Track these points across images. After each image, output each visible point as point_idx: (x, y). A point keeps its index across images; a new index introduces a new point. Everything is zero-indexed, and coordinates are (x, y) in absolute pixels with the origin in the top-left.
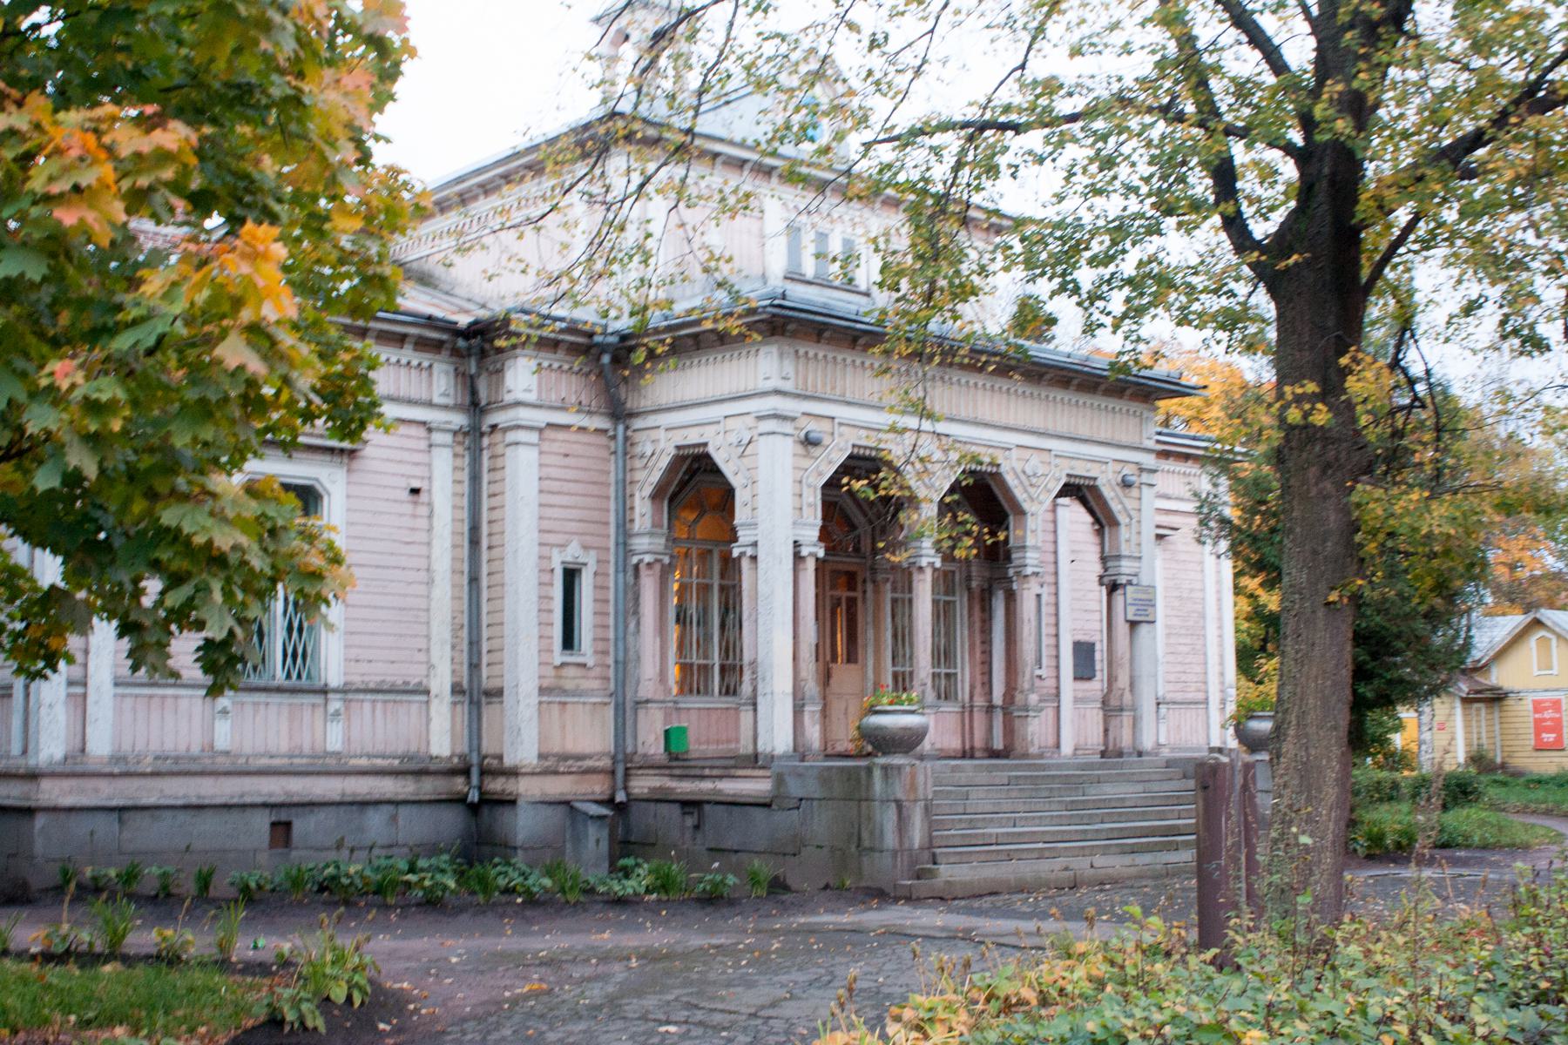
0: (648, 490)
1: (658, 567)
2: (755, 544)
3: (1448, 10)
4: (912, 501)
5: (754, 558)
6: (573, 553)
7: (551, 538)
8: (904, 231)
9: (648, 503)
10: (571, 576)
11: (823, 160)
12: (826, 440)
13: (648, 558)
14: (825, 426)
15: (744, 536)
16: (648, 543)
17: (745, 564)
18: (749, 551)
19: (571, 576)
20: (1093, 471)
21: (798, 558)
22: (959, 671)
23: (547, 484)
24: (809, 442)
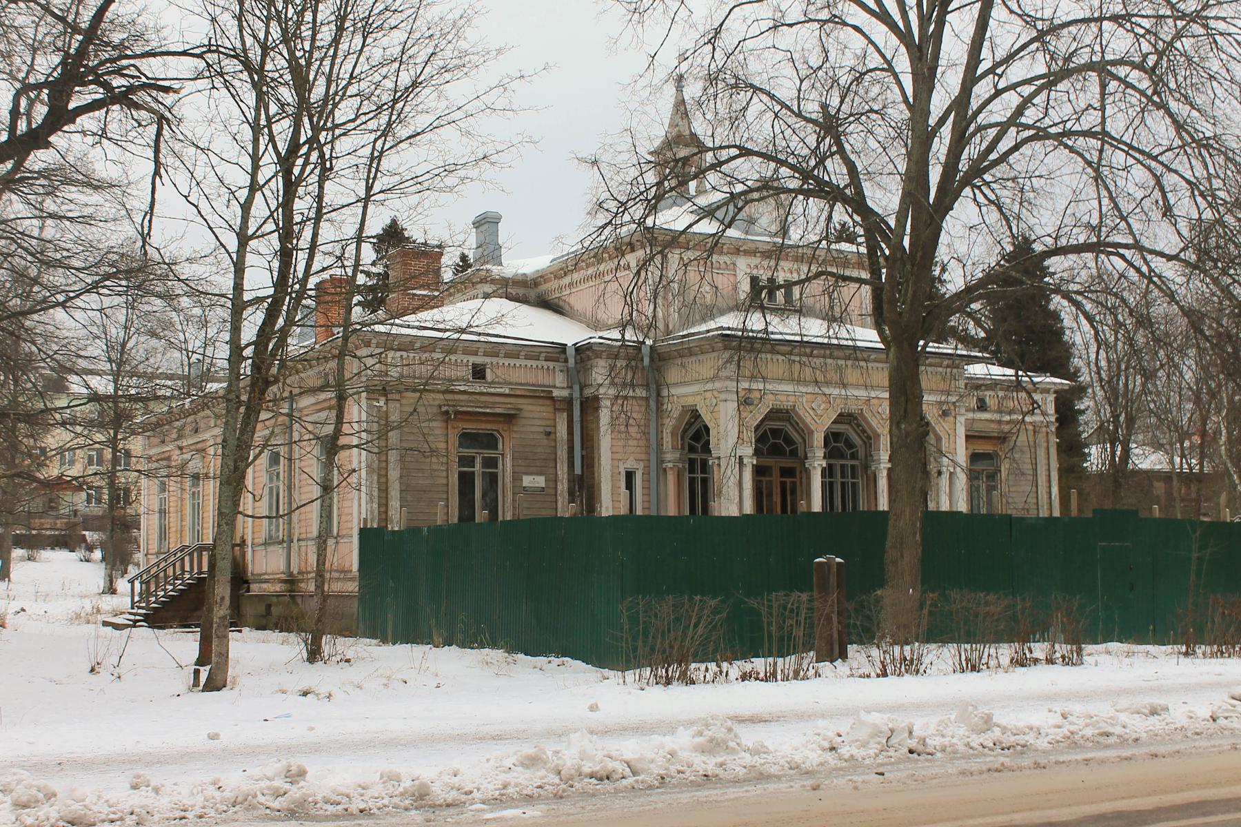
1: (676, 469)
2: (719, 458)
6: (630, 464)
9: (670, 435)
10: (630, 476)
13: (670, 465)
16: (671, 456)
19: (630, 476)
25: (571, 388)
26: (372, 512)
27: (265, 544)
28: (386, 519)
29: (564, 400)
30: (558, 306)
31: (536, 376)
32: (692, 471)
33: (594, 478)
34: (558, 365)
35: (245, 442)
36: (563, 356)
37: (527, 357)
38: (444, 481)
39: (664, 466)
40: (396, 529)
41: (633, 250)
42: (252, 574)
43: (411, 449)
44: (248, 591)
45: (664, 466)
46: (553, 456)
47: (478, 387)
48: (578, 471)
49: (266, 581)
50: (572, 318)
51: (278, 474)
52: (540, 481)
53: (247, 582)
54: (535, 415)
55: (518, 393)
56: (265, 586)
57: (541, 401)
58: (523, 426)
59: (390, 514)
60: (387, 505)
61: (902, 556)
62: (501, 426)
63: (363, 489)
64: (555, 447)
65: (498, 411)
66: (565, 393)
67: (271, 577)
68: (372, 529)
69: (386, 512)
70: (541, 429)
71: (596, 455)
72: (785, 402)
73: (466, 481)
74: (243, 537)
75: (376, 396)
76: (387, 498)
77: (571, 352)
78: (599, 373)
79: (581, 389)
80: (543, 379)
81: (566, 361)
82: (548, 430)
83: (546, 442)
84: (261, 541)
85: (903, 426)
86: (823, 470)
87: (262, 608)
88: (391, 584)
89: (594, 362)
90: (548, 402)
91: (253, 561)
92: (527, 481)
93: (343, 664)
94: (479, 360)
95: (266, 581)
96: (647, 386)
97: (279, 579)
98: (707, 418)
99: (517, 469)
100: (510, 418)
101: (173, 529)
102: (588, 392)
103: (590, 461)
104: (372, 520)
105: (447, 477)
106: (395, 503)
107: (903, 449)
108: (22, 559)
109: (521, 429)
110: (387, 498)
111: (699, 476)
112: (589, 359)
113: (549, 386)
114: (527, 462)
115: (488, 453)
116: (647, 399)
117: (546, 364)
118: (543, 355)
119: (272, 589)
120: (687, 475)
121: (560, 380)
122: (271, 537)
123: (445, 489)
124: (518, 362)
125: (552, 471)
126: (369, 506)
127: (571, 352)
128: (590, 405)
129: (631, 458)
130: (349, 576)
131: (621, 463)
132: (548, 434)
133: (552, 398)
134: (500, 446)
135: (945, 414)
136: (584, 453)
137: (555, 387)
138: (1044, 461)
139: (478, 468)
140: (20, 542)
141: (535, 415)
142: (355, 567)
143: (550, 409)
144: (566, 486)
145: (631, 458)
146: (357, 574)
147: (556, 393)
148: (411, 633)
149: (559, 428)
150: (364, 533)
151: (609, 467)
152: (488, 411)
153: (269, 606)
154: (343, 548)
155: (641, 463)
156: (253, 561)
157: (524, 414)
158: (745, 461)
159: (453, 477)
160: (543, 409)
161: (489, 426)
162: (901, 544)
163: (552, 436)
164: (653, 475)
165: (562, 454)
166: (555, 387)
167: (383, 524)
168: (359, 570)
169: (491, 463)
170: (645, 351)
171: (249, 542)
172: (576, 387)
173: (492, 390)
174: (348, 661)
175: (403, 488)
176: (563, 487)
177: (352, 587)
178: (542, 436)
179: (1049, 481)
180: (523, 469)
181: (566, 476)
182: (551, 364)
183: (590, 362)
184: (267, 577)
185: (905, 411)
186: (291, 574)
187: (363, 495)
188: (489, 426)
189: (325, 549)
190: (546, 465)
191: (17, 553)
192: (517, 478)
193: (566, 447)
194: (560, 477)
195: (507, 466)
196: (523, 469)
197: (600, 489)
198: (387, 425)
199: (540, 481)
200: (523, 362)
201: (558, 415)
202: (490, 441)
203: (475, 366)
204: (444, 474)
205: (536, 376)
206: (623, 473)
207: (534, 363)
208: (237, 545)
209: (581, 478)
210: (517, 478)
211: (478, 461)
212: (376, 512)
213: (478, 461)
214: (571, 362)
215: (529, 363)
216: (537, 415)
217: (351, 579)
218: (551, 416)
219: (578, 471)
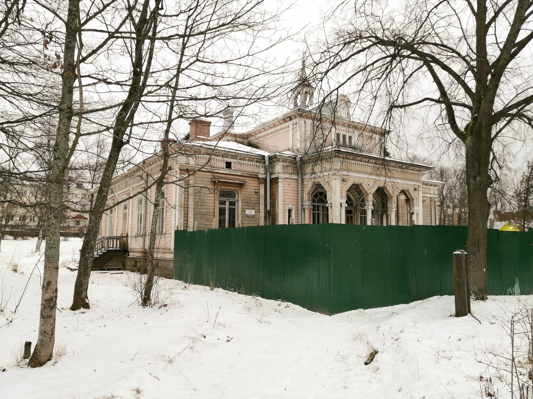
0: (306, 192)
1: (309, 209)
2: (331, 204)
3: (68, 1)
4: (367, 194)
5: (331, 207)
6: (290, 206)
7: (285, 203)
8: (6, 66)
9: (307, 195)
10: (290, 211)
11: (157, 78)
12: (348, 180)
13: (307, 207)
14: (347, 177)
15: (329, 202)
16: (307, 203)
17: (329, 208)
18: (330, 205)
19: (290, 211)
20: (361, 181)
21: (341, 206)
22: (236, 207)
23: (424, 213)
24: (343, 180)
25: (266, 174)
26: (181, 223)
27: (135, 237)
28: (187, 227)
29: (263, 179)
30: (257, 145)
31: (252, 168)
32: (313, 210)
33: (275, 212)
34: (261, 165)
35: (108, 176)
36: (263, 161)
37: (249, 160)
38: (213, 211)
39: (304, 207)
40: (191, 231)
41: (291, 120)
42: (130, 249)
43: (204, 187)
44: (128, 255)
45: (304, 207)
46: (258, 202)
47: (227, 171)
48: (268, 208)
49: (136, 252)
50: (262, 150)
51: (141, 208)
52: (253, 212)
53: (128, 252)
54: (251, 185)
55: (245, 175)
56: (135, 254)
57: (253, 179)
58: (246, 189)
59: (189, 224)
60: (187, 220)
61: (479, 250)
62: (237, 188)
63: (177, 208)
64: (259, 198)
65: (236, 182)
66: (264, 176)
67: (137, 250)
68: (181, 231)
69: (187, 224)
70: (254, 191)
71: (276, 202)
72: (357, 182)
73: (222, 212)
74: (127, 234)
75: (184, 172)
76: (187, 217)
77: (267, 159)
78: (279, 167)
79: (270, 175)
80: (255, 170)
81: (265, 163)
82: (257, 191)
83: (255, 196)
84: (133, 235)
85: (478, 179)
86: (372, 211)
87: (133, 263)
88: (189, 256)
89: (276, 164)
90: (256, 180)
91: (131, 243)
92: (248, 212)
93: (163, 309)
94: (229, 160)
95: (136, 252)
96: (298, 174)
97: (140, 251)
98: (326, 187)
99: (244, 207)
100: (241, 185)
101: (103, 231)
102: (273, 176)
103: (273, 205)
104: (181, 227)
105: (214, 209)
106: (191, 220)
107: (478, 192)
108: (63, 240)
109: (246, 190)
110: (187, 217)
111: (317, 212)
112: (274, 162)
113: (257, 173)
114: (248, 204)
115: (232, 200)
116: (297, 179)
117: (256, 163)
118: (255, 160)
119: (137, 255)
120: (312, 212)
121: (262, 170)
122: (138, 234)
123: (213, 214)
124: (245, 162)
125: (257, 208)
126: (179, 220)
127: (267, 159)
128: (274, 181)
129: (291, 204)
130: (170, 251)
131: (287, 205)
132: (256, 193)
133: (258, 178)
134: (237, 197)
135: (415, 189)
136: (271, 201)
137: (259, 173)
138: (434, 212)
139: (227, 206)
140: (62, 234)
141: (251, 185)
142: (172, 247)
143: (257, 182)
144: (263, 215)
145: (291, 204)
146: (173, 251)
147: (260, 176)
148: (198, 280)
149: (261, 190)
150: (177, 232)
151: (282, 207)
152: (232, 181)
153: (136, 262)
154: (168, 239)
155: (295, 206)
156: (131, 243)
157: (247, 184)
158: (343, 205)
159: (217, 209)
160: (254, 182)
161: (232, 188)
162: (478, 243)
163: (258, 194)
164: (300, 211)
165: (262, 201)
166: (259, 173)
167: (186, 229)
168: (174, 249)
169: (232, 204)
170: (298, 159)
171: (129, 236)
172: (268, 174)
173: (234, 173)
174: (166, 305)
175: (195, 213)
176: (262, 214)
177: (171, 256)
178: (254, 194)
179: (435, 219)
180: (246, 207)
181: (263, 210)
182: (258, 164)
183: (274, 164)
184: (136, 250)
185: (479, 170)
186: (145, 249)
187: (177, 211)
188: (232, 188)
189: (154, 240)
190: (255, 206)
191: (62, 238)
192: (243, 210)
193: (263, 198)
194: (261, 211)
195: (239, 206)
196: (246, 207)
197: (278, 216)
198: (188, 185)
199: (253, 212)
200: (247, 162)
201: (261, 185)
202: (231, 194)
203: (227, 163)
204: (213, 208)
205: (252, 168)
206: (287, 210)
207: (251, 163)
208: (125, 237)
209: (269, 212)
210: (243, 210)
211: (227, 203)
212: (183, 223)
213: (227, 203)
214: (267, 163)
215: (249, 163)
216: (252, 185)
217: (171, 253)
218: (258, 185)
219: (268, 208)
